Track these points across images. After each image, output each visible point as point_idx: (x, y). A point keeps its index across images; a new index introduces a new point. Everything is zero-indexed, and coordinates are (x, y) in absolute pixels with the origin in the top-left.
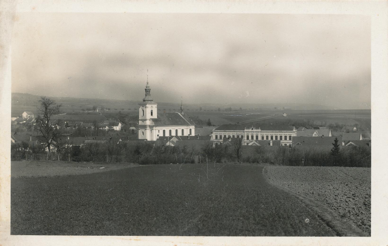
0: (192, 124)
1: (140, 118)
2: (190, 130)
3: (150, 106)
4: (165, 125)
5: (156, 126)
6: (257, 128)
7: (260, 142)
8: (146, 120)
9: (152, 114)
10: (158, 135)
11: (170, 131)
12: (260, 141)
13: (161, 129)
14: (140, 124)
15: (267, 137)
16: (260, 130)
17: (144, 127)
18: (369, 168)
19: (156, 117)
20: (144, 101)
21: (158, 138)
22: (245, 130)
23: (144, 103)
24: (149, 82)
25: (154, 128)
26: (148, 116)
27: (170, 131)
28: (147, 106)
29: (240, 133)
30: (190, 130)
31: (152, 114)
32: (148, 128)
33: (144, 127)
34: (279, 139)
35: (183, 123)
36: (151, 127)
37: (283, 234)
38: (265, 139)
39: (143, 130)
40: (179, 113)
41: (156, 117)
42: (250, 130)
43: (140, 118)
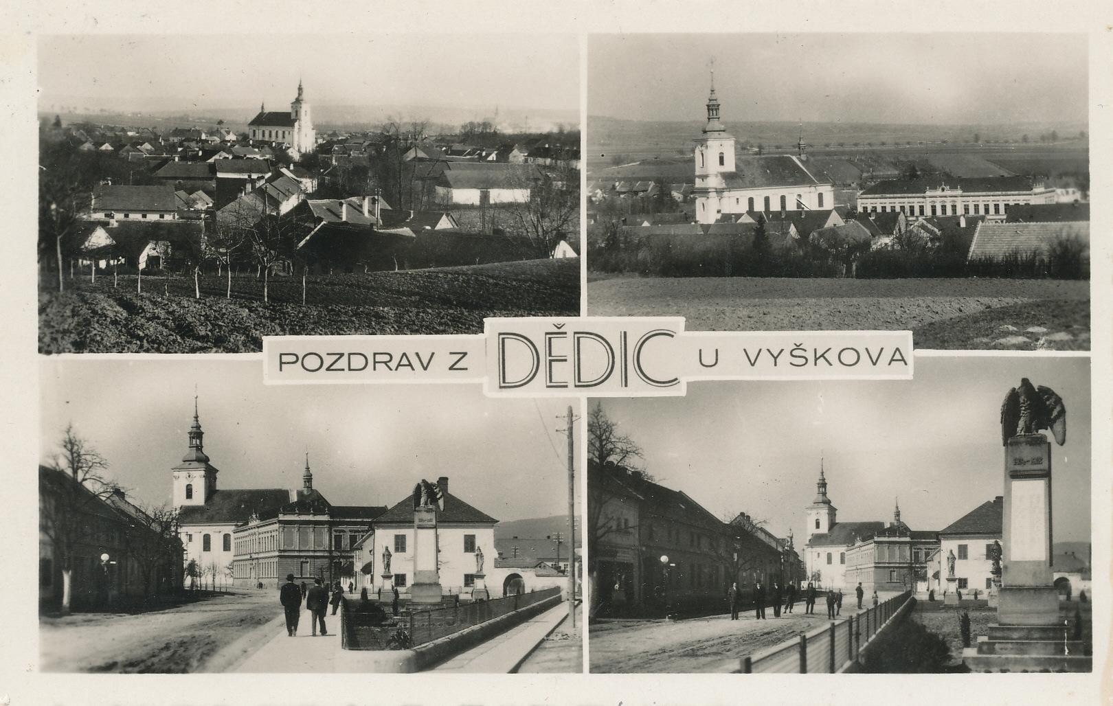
0: (823, 179)
1: (698, 172)
2: (820, 196)
3: (717, 143)
4: (753, 185)
5: (729, 189)
6: (953, 187)
7: (759, 218)
8: (706, 176)
9: (722, 163)
10: (719, 212)
11: (767, 200)
12: (938, 218)
13: (744, 195)
14: (697, 186)
15: (976, 207)
16: (959, 192)
17: (705, 192)
18: (1081, 283)
19: (733, 169)
20: (705, 132)
21: (719, 216)
22: (928, 193)
23: (705, 136)
24: (716, 87)
25: (726, 194)
26: (713, 167)
27: (767, 200)
28: (709, 143)
29: (906, 200)
30: (820, 196)
31: (722, 163)
32: (713, 195)
33: (705, 192)
34: (982, 212)
35: (797, 178)
36: (719, 192)
37: (278, 329)
38: (949, 212)
39: (703, 200)
40: (794, 158)
41: (733, 169)
42: (939, 192)
43: (697, 173)
